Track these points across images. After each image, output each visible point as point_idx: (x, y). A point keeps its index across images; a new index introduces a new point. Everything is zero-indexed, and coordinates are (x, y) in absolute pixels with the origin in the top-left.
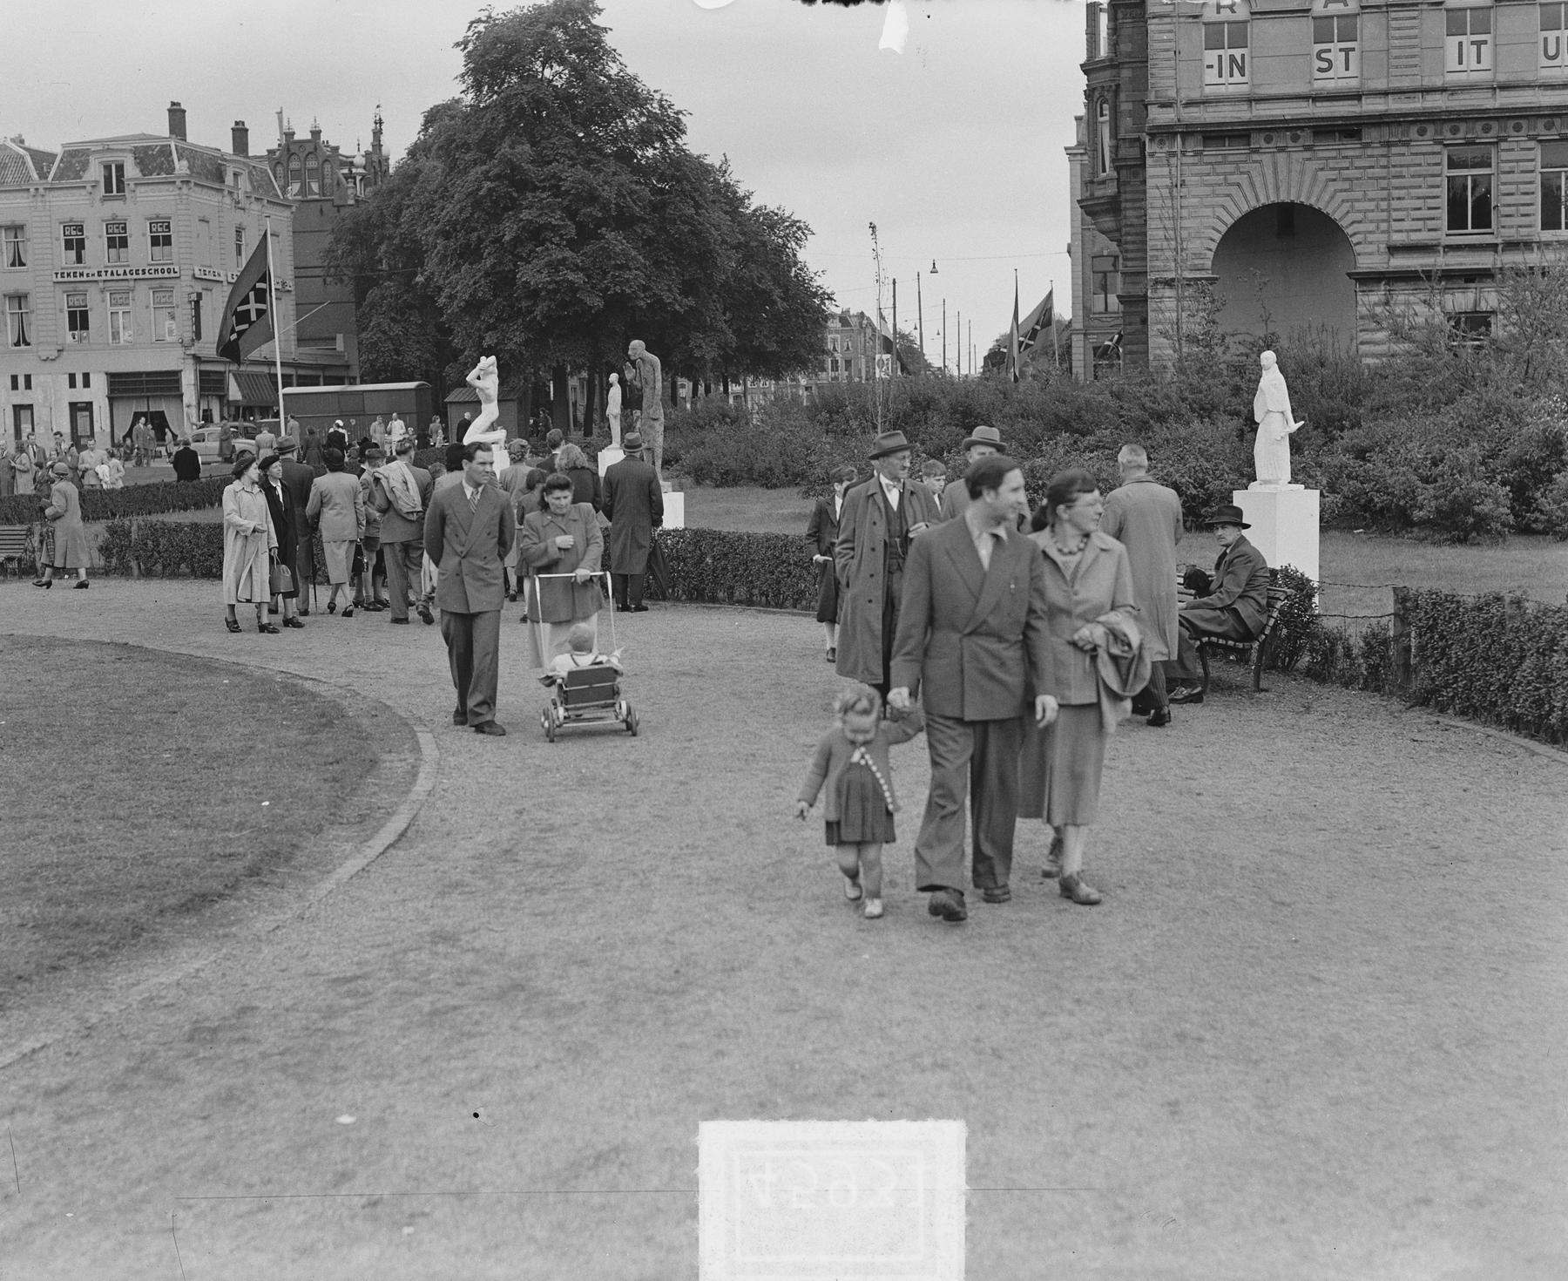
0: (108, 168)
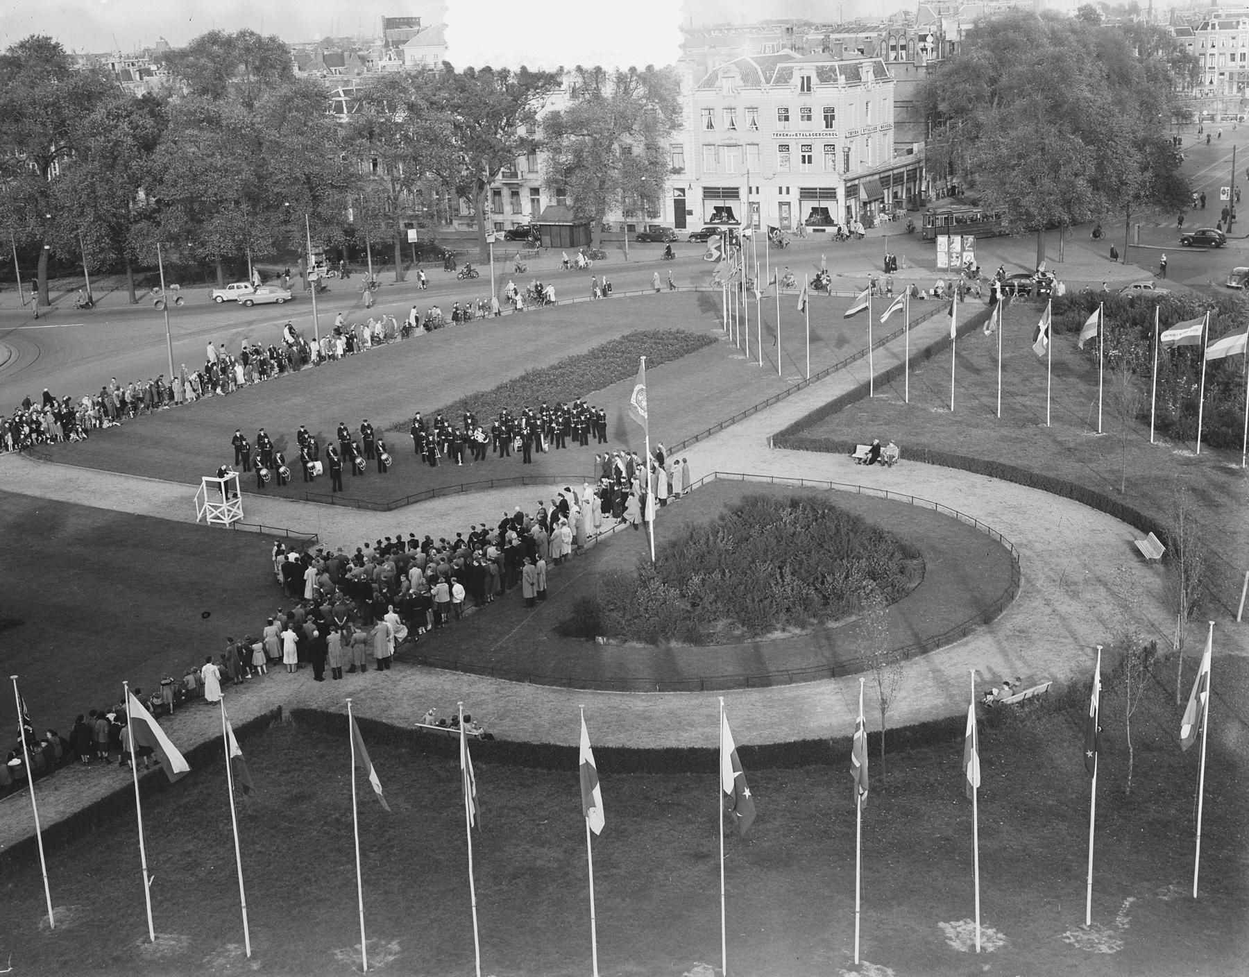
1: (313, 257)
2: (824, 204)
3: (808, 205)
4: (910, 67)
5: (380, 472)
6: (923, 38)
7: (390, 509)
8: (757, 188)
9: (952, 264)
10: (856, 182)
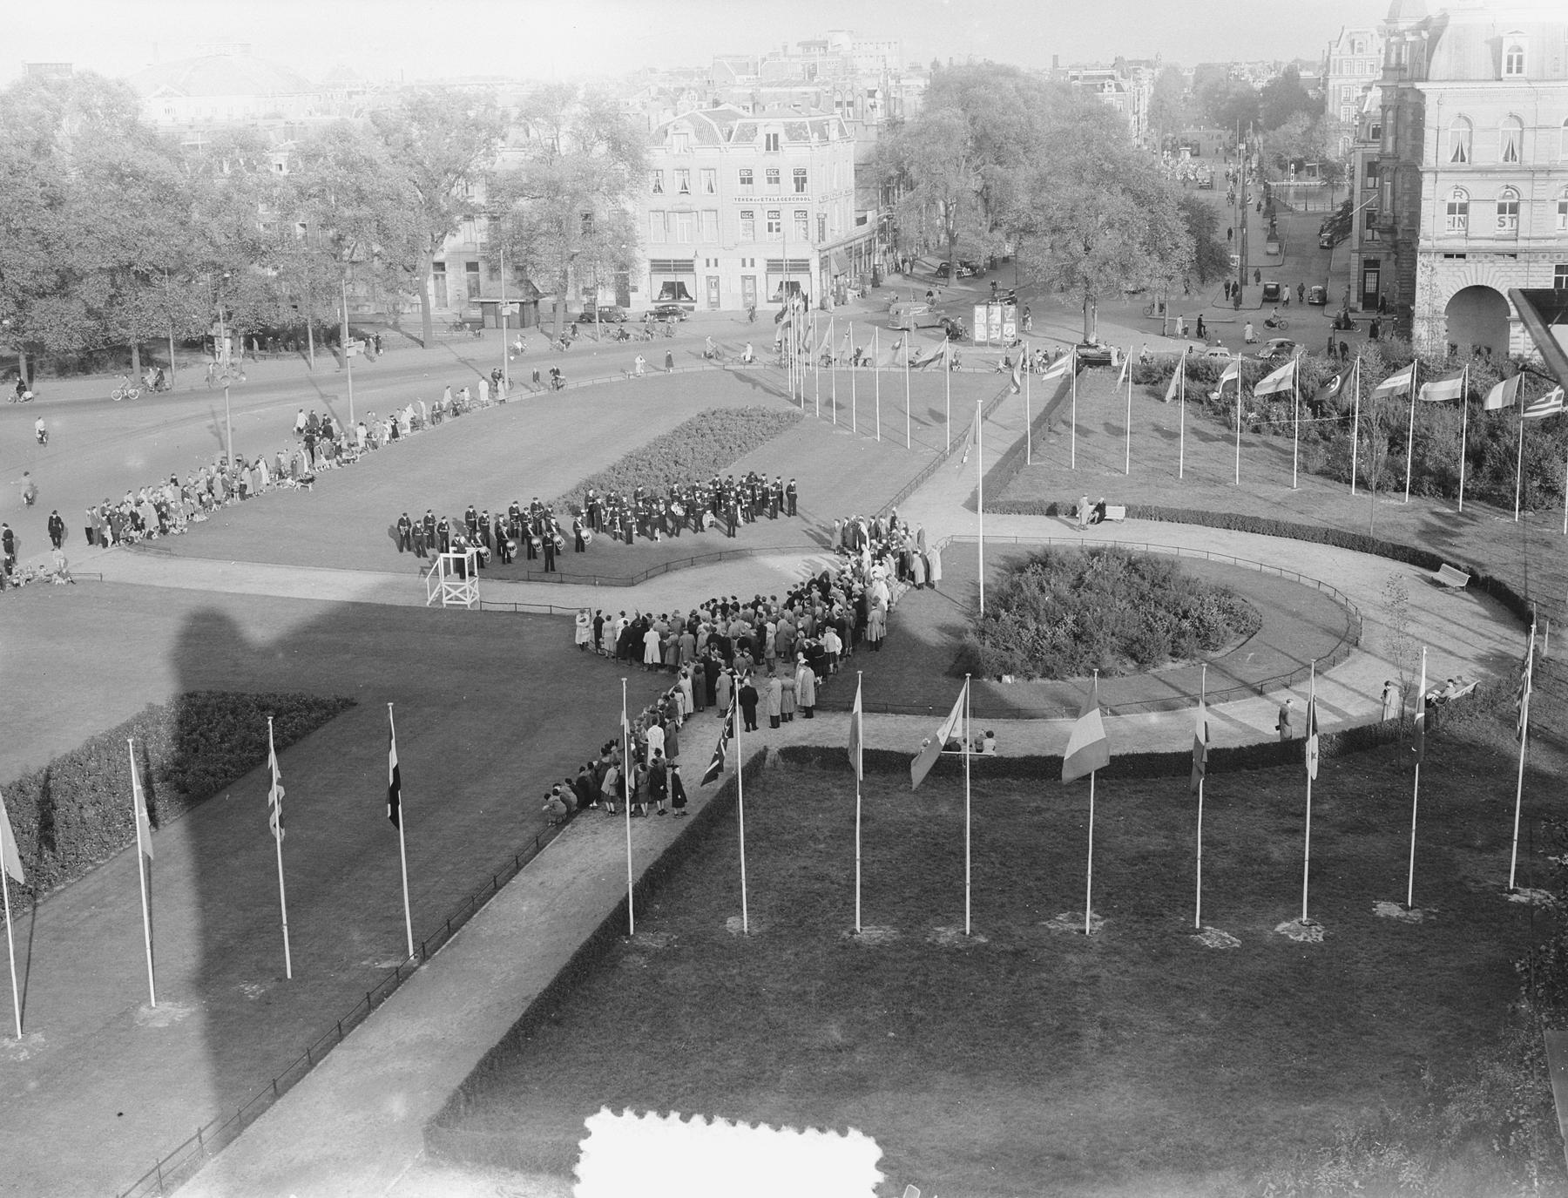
0: (768, 136)
1: (228, 341)
2: (794, 278)
3: (776, 279)
4: (859, 126)
5: (529, 558)
6: (872, 94)
7: (633, 585)
8: (716, 260)
9: (992, 337)
10: (827, 253)
